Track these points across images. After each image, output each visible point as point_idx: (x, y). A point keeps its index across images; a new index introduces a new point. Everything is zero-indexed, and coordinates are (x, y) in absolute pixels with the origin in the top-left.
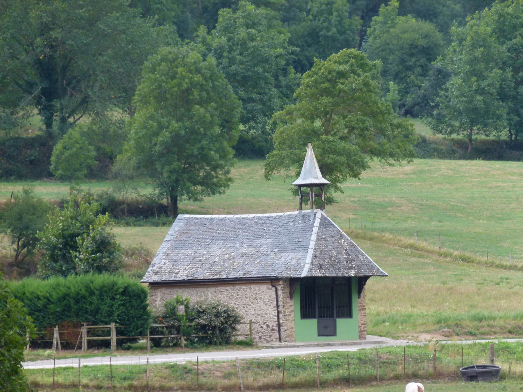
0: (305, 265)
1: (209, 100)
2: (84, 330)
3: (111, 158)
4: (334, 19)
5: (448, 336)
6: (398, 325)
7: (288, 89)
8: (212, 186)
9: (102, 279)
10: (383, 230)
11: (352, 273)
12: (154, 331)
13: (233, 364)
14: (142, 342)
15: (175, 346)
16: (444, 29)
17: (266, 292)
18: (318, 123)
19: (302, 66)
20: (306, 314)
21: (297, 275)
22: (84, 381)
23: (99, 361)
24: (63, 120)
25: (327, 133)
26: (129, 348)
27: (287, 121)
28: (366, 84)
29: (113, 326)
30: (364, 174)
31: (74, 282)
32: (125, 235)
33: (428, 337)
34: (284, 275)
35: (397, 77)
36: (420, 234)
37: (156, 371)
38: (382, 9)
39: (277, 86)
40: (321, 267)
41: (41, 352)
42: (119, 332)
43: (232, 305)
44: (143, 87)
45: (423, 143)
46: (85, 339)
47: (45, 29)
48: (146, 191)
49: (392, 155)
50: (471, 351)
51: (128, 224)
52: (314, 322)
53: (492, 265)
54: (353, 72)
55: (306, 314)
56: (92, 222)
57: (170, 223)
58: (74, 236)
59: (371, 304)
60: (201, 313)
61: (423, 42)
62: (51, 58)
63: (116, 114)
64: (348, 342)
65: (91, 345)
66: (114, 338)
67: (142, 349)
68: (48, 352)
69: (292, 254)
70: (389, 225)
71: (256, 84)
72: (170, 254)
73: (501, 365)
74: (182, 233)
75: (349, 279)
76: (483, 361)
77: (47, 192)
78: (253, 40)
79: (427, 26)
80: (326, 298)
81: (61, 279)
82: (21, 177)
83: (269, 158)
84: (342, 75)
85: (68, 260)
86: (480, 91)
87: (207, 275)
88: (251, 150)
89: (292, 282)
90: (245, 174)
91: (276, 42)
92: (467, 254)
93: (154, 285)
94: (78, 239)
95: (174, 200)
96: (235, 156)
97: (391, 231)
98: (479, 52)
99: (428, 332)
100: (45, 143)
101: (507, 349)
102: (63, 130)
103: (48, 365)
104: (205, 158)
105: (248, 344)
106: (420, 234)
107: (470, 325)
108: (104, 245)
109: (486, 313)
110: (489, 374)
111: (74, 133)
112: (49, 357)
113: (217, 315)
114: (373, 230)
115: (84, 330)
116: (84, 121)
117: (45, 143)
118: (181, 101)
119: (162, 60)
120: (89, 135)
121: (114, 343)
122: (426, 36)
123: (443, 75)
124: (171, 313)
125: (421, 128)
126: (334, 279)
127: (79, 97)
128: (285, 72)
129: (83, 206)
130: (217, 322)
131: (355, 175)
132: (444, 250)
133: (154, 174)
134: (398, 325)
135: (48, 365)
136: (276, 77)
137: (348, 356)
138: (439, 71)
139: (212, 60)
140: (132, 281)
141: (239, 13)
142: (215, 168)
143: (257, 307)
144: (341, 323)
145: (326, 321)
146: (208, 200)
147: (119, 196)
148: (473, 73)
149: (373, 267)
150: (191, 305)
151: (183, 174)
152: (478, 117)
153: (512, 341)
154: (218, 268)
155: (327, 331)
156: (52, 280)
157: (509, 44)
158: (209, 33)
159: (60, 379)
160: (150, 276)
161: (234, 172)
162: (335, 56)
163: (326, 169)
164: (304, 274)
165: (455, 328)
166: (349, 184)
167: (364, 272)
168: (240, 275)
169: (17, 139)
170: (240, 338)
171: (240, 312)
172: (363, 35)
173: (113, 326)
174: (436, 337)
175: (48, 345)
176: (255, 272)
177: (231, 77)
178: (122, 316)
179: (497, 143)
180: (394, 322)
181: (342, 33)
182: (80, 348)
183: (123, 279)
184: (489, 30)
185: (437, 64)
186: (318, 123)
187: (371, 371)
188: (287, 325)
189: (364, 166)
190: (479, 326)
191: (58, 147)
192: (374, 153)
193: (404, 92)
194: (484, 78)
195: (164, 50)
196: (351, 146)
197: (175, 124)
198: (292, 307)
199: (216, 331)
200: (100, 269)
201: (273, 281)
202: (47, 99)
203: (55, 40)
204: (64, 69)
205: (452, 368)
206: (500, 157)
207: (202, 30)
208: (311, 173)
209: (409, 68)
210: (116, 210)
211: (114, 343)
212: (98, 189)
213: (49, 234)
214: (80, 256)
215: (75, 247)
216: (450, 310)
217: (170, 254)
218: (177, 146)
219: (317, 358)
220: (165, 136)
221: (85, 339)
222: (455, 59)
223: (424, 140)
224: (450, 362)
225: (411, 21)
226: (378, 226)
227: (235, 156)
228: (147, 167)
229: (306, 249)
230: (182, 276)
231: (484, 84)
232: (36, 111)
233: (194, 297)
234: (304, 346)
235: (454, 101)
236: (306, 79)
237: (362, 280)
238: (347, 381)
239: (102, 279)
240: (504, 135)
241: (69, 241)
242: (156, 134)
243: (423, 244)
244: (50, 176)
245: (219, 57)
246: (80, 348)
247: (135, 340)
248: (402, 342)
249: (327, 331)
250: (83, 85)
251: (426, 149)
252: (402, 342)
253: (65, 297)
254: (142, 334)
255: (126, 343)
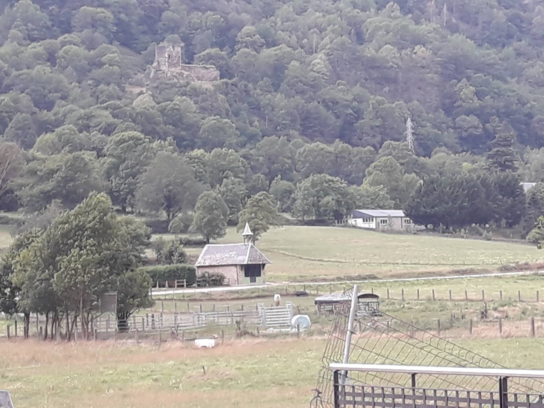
0: (245, 260)
1: (219, 208)
2: (176, 282)
3: (189, 226)
4: (260, 181)
5: (291, 282)
6: (276, 278)
7: (55, 228)
8: (220, 235)
9: (181, 265)
10: (274, 249)
11: (261, 263)
12: (198, 282)
13: (223, 292)
14: (194, 285)
15: (205, 286)
16: (295, 185)
17: (234, 269)
18: (253, 215)
19: (249, 197)
20: (246, 276)
21: (242, 263)
22: (175, 298)
23: (180, 291)
24: (173, 215)
25: (256, 218)
26: (190, 287)
27: (244, 214)
28: (268, 203)
29: (185, 280)
30: (268, 231)
31: (173, 266)
32: (189, 251)
33: (285, 282)
34: (239, 263)
35: (281, 200)
36: (285, 250)
37: (438, 168)
38: (276, 178)
39: (242, 203)
40: (251, 261)
41: (161, 289)
42: (187, 282)
43: (223, 273)
44: (198, 204)
45: (288, 220)
46: (176, 284)
47: (167, 186)
48: (200, 237)
49: (277, 225)
50: (298, 287)
51: (193, 248)
52: (249, 278)
53: (308, 259)
54: (264, 199)
55: (246, 276)
56: (178, 247)
57: (203, 248)
58: (173, 252)
59: (267, 272)
60: (213, 276)
61: (289, 189)
62: (169, 195)
63: (190, 213)
64: (260, 284)
65: (178, 286)
66: (185, 284)
67: (194, 287)
68: (164, 289)
69: (241, 257)
70: (276, 247)
71: (235, 203)
72: (205, 257)
73: (307, 291)
74: (207, 250)
75: (260, 265)
76: (302, 290)
77: (167, 237)
78: (234, 188)
79: (291, 184)
80: (252, 270)
81: (168, 266)
82: (160, 233)
83: (238, 225)
84: (261, 200)
85: (171, 259)
86: (306, 204)
87: (215, 264)
88: (232, 223)
89: (242, 266)
90: (230, 231)
91: (241, 190)
92: (301, 256)
93: (199, 267)
94: (174, 253)
95: (208, 240)
96: (227, 226)
97: (276, 249)
98: (306, 192)
99: (285, 281)
100: (167, 222)
101: (310, 286)
102: (173, 218)
103: (164, 293)
104: (217, 226)
105: (228, 285)
106: (285, 250)
107: (298, 278)
108: (182, 255)
109: (304, 275)
110: (304, 294)
111: (176, 219)
112: (165, 290)
113: (218, 276)
114: (271, 248)
115: (176, 282)
116: (180, 215)
117: (167, 222)
118: (210, 209)
119: (205, 196)
120: (181, 220)
121: (185, 286)
122: (290, 187)
123: (294, 200)
124: (204, 276)
125: (287, 216)
126: (255, 264)
127: (178, 208)
128: (244, 199)
129: (175, 242)
130: (218, 278)
131: (265, 231)
132: (293, 255)
133: (202, 232)
134: (276, 278)
135: (164, 293)
136: (241, 200)
137: (259, 289)
138: (293, 198)
139: (220, 195)
140: (190, 266)
141: (230, 180)
142: (221, 229)
143: (231, 274)
144: (257, 278)
145: (253, 278)
146: (219, 240)
147: (191, 239)
148: (304, 198)
149: (267, 261)
150: (210, 273)
151: (211, 231)
152: (306, 212)
153: (312, 284)
154: (218, 262)
155: (253, 281)
156: (166, 266)
157: (316, 189)
158: (220, 186)
159: (167, 297)
160: (197, 264)
161: (227, 230)
162: (258, 194)
163: (253, 230)
164: (245, 263)
165: (295, 280)
166: (263, 234)
167: (264, 263)
168: (225, 263)
169: (159, 221)
170: (225, 284)
171: (225, 275)
172: (269, 187)
173: (185, 280)
174: (287, 283)
175: (164, 286)
176: (230, 262)
177: (226, 201)
178: (188, 278)
179: (312, 220)
180: (275, 278)
181: (262, 186)
182: (174, 287)
183: (187, 265)
184: (309, 185)
185: (292, 196)
186: (253, 215)
187: (266, 293)
188: (240, 279)
189: (268, 228)
190: (303, 278)
191: (171, 224)
192: (271, 224)
193: (282, 205)
194: (307, 200)
195: (205, 192)
196: (264, 222)
197: (209, 216)
198: (242, 273)
199: (218, 281)
200: (181, 262)
201: (236, 265)
202: (168, 208)
203: (170, 189)
204: (174, 198)
205: (292, 292)
206: (313, 225)
207: (218, 186)
208: (247, 231)
209: (285, 197)
210: (188, 243)
211: (185, 286)
212: (183, 236)
213: (165, 250)
214: (175, 258)
215: (173, 255)
216: (293, 274)
217: (205, 257)
218: (209, 222)
219: (249, 290)
220: (205, 220)
221: (176, 284)
222: (298, 195)
223: (288, 220)
224: (291, 291)
225: (285, 182)
226: (273, 247)
227: (227, 226)
228: (199, 229)
229: (246, 255)
230: (207, 264)
231: (308, 202)
232: (164, 212)
233: (211, 271)
234: (246, 285)
235: (298, 208)
236: (249, 202)
237: (264, 265)
238: (258, 297)
239: (181, 265)
240: (314, 218)
241: (171, 254)
242: (203, 219)
243: (287, 253)
244: (169, 232)
245: (223, 196)
246: (174, 287)
247: (192, 285)
248: (277, 284)
249: (253, 281)
250: (180, 204)
251: (288, 223)
252: (277, 284)
253: (170, 271)
254: (194, 283)
255: (189, 286)
